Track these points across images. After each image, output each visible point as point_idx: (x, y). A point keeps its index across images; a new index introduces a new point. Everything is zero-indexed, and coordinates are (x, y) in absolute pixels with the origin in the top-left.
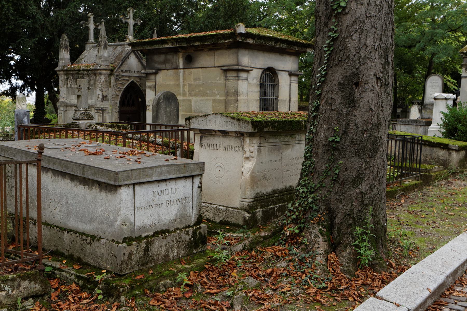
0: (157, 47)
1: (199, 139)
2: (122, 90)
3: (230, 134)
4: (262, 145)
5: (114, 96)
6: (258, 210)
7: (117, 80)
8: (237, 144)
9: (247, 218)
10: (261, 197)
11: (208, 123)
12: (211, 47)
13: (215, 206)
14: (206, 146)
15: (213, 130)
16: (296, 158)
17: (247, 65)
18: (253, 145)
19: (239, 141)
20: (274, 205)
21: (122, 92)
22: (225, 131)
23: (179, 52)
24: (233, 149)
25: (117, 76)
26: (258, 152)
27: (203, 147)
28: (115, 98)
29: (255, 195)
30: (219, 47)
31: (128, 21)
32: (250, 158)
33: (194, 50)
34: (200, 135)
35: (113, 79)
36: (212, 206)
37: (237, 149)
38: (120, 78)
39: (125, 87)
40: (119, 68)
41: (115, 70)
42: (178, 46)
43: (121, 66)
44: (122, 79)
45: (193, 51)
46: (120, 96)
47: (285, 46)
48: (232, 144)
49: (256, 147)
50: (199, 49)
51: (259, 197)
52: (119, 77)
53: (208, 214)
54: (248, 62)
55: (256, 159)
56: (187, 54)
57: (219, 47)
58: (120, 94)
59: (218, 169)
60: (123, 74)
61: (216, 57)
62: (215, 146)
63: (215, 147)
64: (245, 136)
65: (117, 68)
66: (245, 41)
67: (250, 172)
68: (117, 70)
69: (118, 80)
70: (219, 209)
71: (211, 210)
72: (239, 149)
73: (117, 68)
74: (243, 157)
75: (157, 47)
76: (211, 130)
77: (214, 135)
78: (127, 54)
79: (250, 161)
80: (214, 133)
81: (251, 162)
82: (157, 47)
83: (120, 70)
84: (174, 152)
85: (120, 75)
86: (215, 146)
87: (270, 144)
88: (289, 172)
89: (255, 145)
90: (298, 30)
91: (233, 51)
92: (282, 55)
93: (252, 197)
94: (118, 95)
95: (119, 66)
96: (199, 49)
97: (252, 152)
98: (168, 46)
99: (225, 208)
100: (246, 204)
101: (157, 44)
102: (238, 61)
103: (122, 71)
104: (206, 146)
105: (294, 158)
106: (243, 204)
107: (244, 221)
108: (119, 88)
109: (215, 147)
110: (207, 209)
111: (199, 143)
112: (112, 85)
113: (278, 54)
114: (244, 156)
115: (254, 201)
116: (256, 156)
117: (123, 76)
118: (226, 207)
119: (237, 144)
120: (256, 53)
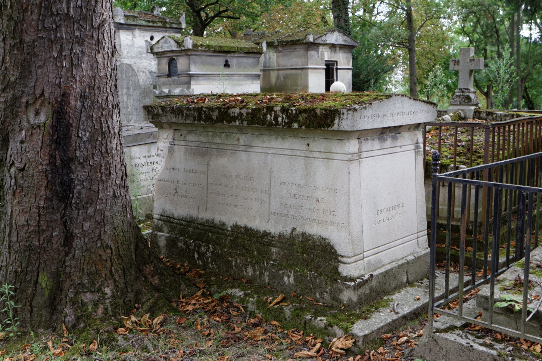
4: (176, 142)
26: (169, 152)
49: (168, 145)
115: (160, 220)
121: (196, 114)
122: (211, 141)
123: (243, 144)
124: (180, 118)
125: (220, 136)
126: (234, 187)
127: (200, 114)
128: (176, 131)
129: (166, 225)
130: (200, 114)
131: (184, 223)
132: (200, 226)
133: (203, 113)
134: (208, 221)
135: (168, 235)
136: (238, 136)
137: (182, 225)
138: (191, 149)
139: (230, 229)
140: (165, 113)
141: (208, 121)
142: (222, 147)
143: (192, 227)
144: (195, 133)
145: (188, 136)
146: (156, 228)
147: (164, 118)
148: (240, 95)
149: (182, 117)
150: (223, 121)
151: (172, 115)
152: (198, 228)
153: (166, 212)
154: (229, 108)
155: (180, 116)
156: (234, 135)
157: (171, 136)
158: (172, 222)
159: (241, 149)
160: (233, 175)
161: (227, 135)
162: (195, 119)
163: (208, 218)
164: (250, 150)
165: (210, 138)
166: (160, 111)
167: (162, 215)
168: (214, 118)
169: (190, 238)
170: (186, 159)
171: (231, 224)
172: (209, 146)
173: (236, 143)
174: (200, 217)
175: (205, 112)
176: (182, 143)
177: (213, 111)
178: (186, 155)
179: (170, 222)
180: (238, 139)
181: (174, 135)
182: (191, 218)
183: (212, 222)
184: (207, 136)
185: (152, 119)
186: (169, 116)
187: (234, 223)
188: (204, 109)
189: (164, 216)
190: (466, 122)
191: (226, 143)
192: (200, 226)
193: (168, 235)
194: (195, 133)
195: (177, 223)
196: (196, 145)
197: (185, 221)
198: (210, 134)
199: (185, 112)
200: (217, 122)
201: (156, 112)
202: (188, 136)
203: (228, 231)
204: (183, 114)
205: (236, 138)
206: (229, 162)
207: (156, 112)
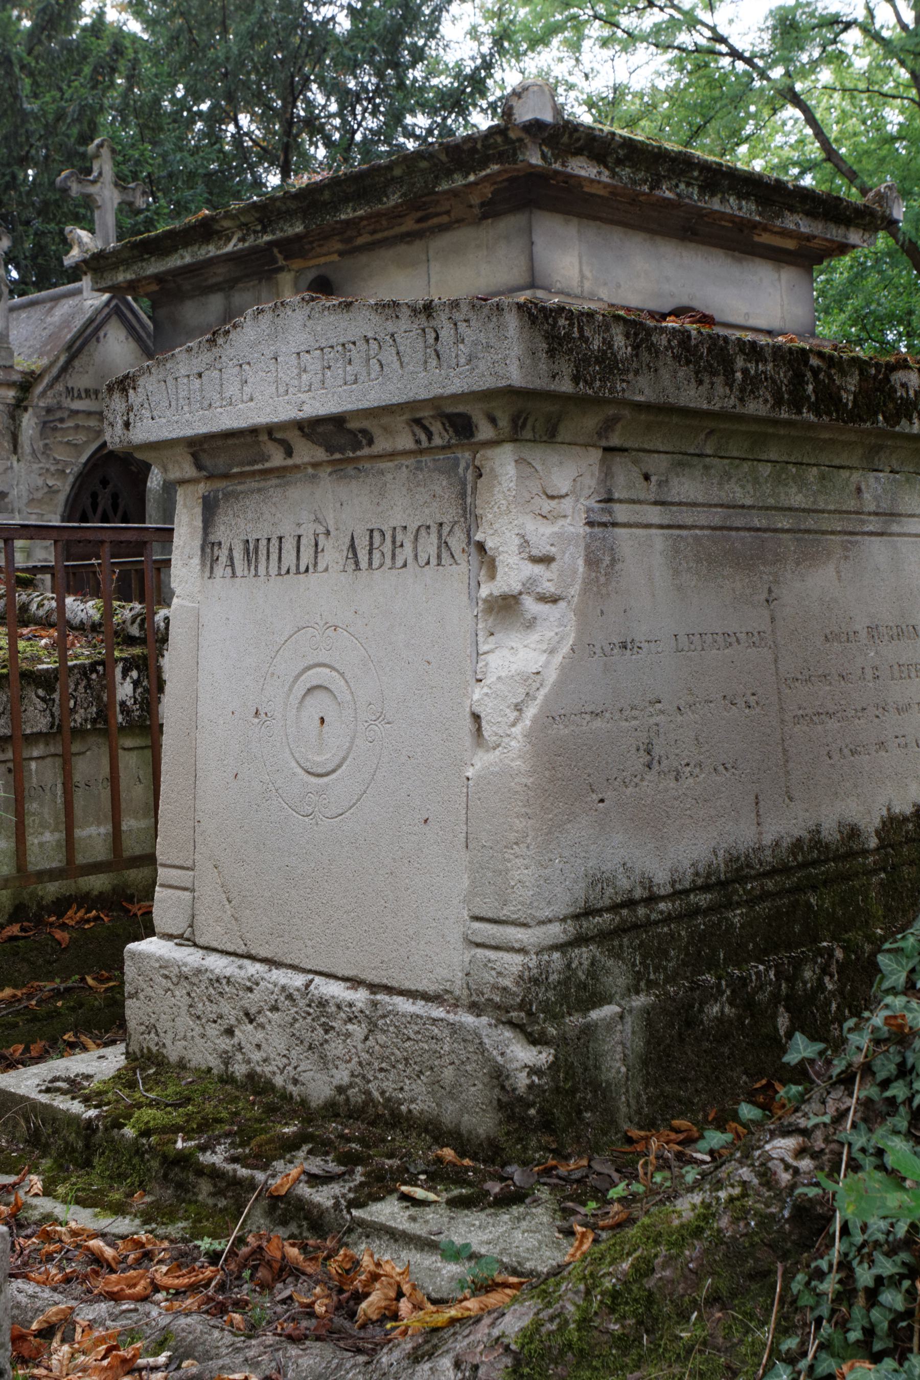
0: (185, 258)
1: (199, 523)
2: (72, 471)
3: (382, 445)
4: (622, 512)
5: (39, 495)
6: (609, 1010)
7: (47, 427)
8: (432, 513)
9: (522, 1081)
10: (631, 903)
11: (232, 390)
12: (409, 225)
13: (299, 980)
14: (238, 555)
15: (270, 430)
16: (872, 630)
17: (578, 291)
18: (547, 506)
19: (441, 485)
20: (775, 1329)
21: (71, 479)
22: (337, 421)
23: (281, 269)
24: (407, 552)
25: (49, 410)
26: (592, 562)
27: (219, 570)
28: (40, 501)
29: (580, 891)
30: (445, 219)
31: (92, 189)
32: (530, 605)
33: (341, 254)
34: (202, 488)
35: (29, 422)
36: (281, 976)
37: (429, 546)
38: (62, 420)
39: (84, 459)
40: (57, 378)
41: (40, 389)
42: (267, 238)
43: (64, 369)
44: (70, 424)
45: (335, 257)
46: (62, 498)
47: (748, 210)
48: (398, 519)
49: (576, 526)
50: (360, 241)
51: (614, 908)
52: (58, 415)
53: (260, 1035)
54: (582, 276)
55: (581, 614)
56: (311, 275)
57: (445, 219)
58: (65, 487)
59: (318, 705)
60: (77, 405)
61: (435, 267)
62: (289, 546)
63: (289, 559)
64: (485, 432)
65: (46, 381)
66: (557, 166)
67: (531, 711)
68: (50, 386)
69: (55, 429)
70: (323, 1003)
71: (275, 1008)
72: (443, 544)
73: (46, 381)
74: (474, 599)
75: (188, 259)
76: (253, 431)
77: (280, 472)
78: (91, 321)
79: (531, 624)
80: (278, 459)
81: (545, 633)
82: (185, 258)
83: (60, 387)
84: (145, 658)
85: (60, 408)
86: (289, 546)
87: (687, 517)
88: (832, 725)
89: (566, 505)
90: (678, 1315)
91: (511, 222)
92: (740, 261)
93: (562, 910)
94: (52, 491)
95: (55, 371)
96: (360, 241)
97: (546, 560)
98: (229, 248)
99: (360, 996)
100: (514, 962)
101: (186, 245)
102: (532, 269)
103: (69, 391)
104: (238, 555)
105: (860, 625)
106: (487, 964)
107: (501, 1106)
108: (57, 462)
109: (289, 559)
110: (252, 1001)
111: (198, 543)
112: (27, 449)
113: (720, 252)
114: (484, 592)
115: (580, 940)
116: (575, 590)
117: (77, 412)
118: (373, 988)
119: (432, 513)
120: (616, 235)
121: (783, 376)
122: (771, 501)
123: (872, 508)
124: (721, 390)
125: (801, 483)
126: (869, 673)
127: (798, 380)
128: (618, 459)
129: (617, 955)
130: (798, 380)
131: (703, 899)
132: (770, 885)
133: (809, 374)
134: (798, 844)
135: (640, 1001)
136: (856, 476)
137: (695, 911)
138: (697, 539)
139: (873, 843)
140: (645, 356)
141: (829, 414)
142: (810, 523)
143: (739, 905)
144: (706, 468)
145: (674, 482)
146: (564, 998)
147: (643, 381)
148: (623, 308)
149: (730, 383)
150: (876, 414)
151: (683, 372)
152: (765, 895)
153: (610, 881)
154: (892, 368)
155: (719, 380)
156: (845, 474)
157: (590, 482)
158: (648, 924)
159: (871, 528)
160: (857, 627)
161: (823, 477)
162: (779, 402)
163: (797, 833)
164: (895, 528)
165: (767, 489)
166: (619, 341)
167: (588, 912)
168: (847, 398)
169: (738, 957)
170: (679, 588)
171: (877, 823)
172: (764, 523)
173: (852, 505)
174: (768, 840)
175: (816, 372)
176: (654, 514)
177: (843, 373)
178: (676, 573)
179: (635, 927)
180: (859, 490)
181: (607, 474)
182: (732, 859)
183: (816, 841)
184: (756, 481)
185: (576, 379)
186: (665, 375)
187: (885, 812)
188: (814, 361)
189: (598, 912)
190: (268, 465)
191: (821, 505)
192: (770, 885)
193: (640, 1001)
194: (706, 468)
195: (668, 919)
196: (717, 521)
197: (706, 888)
198: (765, 470)
199: (740, 362)
200: (855, 416)
201: (596, 344)
202: (674, 482)
203: (865, 852)
204: (729, 373)
205: (853, 488)
206: (839, 579)
207: (596, 344)
